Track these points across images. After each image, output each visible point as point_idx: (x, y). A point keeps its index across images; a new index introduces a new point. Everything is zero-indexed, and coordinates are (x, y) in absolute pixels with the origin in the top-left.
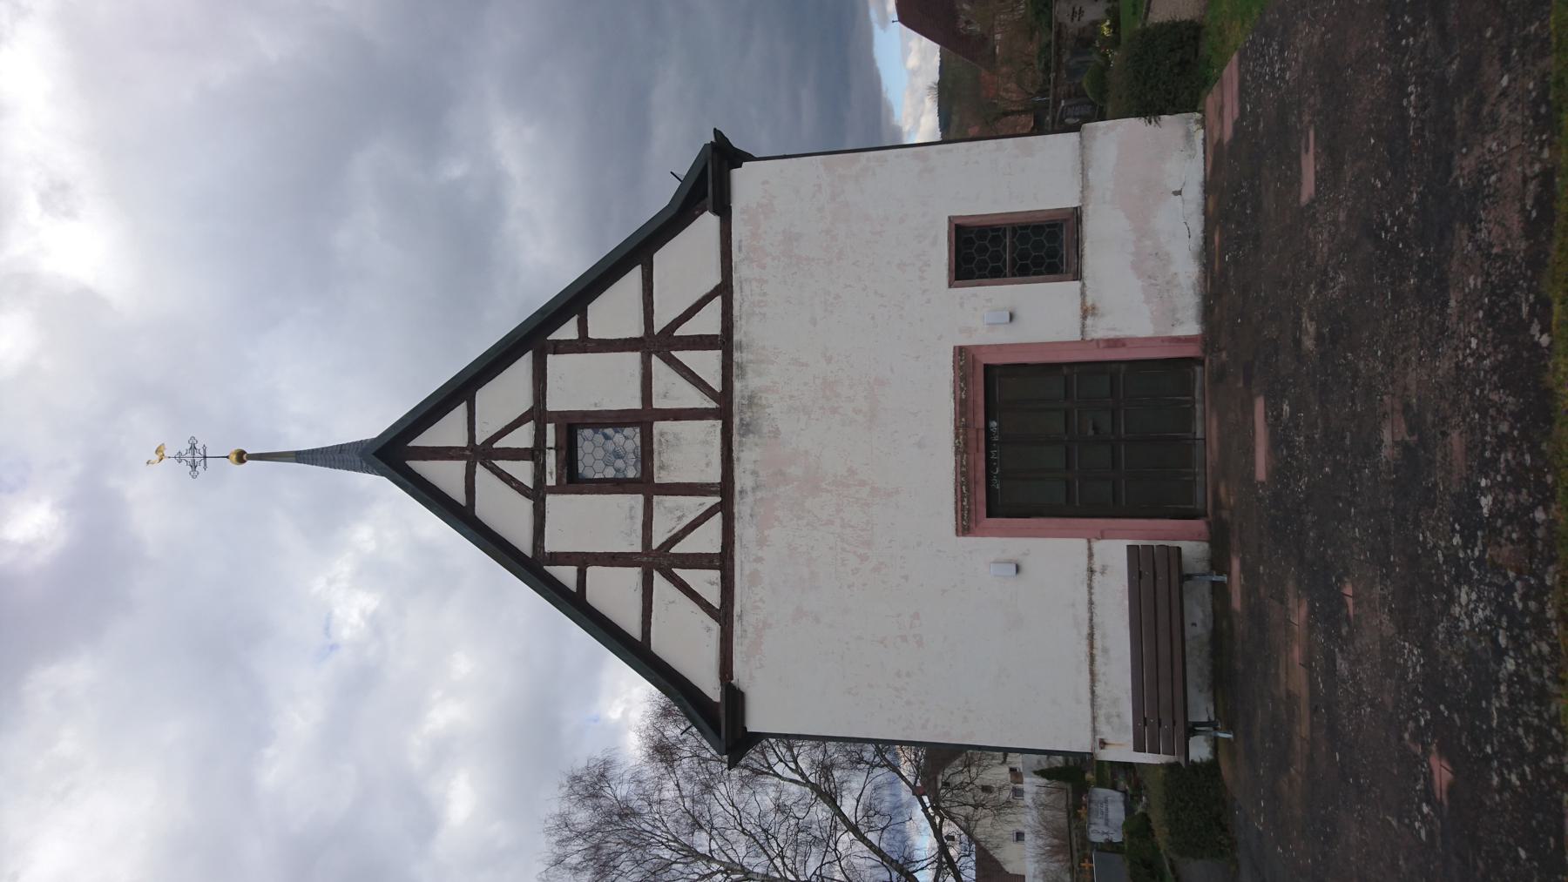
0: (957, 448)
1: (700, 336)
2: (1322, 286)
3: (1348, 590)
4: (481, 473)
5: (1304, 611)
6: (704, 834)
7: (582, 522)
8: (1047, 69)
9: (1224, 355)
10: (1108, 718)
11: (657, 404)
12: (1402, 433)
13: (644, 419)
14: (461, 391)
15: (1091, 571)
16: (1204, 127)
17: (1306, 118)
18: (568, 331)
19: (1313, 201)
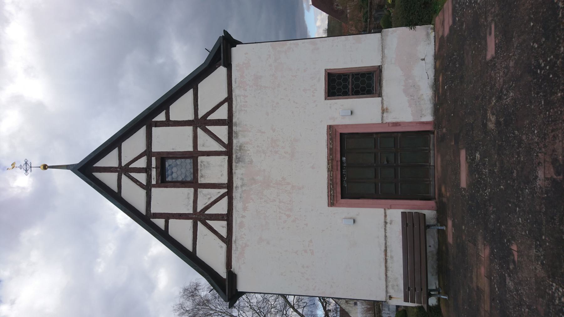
0: (328, 169)
1: (219, 120)
2: (499, 98)
3: (514, 247)
4: (124, 178)
5: (487, 251)
6: (236, 310)
7: (168, 200)
8: (366, 21)
9: (444, 130)
11: (200, 149)
12: (551, 172)
13: (193, 156)
14: (115, 143)
15: (386, 223)
16: (434, 31)
17: (490, 19)
18: (161, 117)
19: (494, 58)
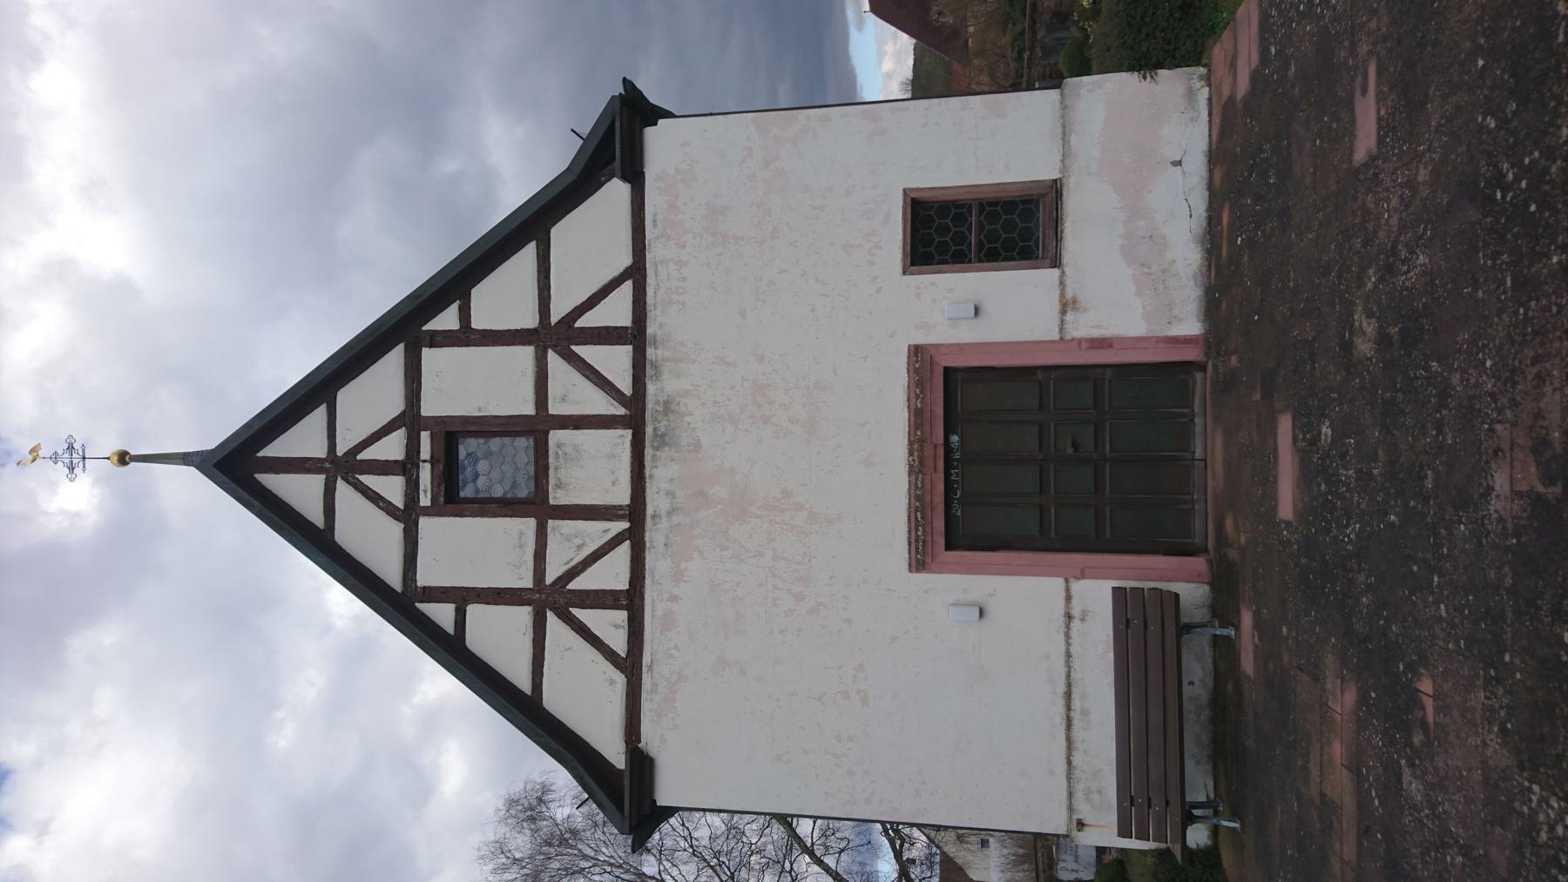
0: (911, 467)
1: (607, 328)
2: (1389, 270)
3: (1426, 686)
4: (342, 488)
5: (1350, 697)
6: (652, 859)
7: (465, 550)
8: (1020, 59)
9: (1234, 360)
10: (1088, 793)
11: (554, 409)
12: (1530, 477)
13: (537, 427)
14: (319, 390)
15: (1069, 617)
16: (1209, 85)
17: (1363, 49)
18: (447, 320)
